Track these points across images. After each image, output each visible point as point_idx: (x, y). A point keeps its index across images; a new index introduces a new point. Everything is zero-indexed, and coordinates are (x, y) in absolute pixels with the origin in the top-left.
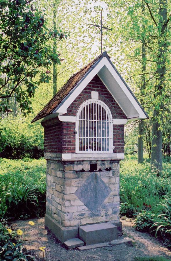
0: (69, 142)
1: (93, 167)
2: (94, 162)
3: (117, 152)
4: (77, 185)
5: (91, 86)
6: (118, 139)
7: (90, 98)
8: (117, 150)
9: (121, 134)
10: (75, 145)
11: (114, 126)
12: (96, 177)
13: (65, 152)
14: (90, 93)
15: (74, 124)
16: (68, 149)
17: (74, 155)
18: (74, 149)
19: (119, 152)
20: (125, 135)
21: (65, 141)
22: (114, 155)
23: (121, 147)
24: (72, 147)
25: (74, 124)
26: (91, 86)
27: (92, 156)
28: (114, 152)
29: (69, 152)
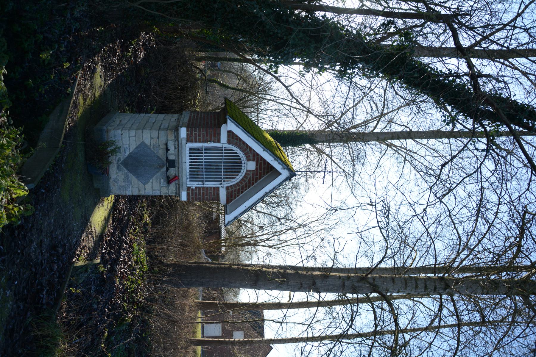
0: (199, 136)
1: (172, 164)
2: (177, 165)
6: (203, 193)
10: (196, 142)
11: (218, 188)
12: (161, 167)
13: (188, 131)
14: (254, 160)
15: (219, 142)
16: (192, 133)
17: (184, 142)
18: (192, 142)
21: (199, 131)
22: (185, 188)
25: (219, 142)
28: (189, 188)
29: (188, 135)
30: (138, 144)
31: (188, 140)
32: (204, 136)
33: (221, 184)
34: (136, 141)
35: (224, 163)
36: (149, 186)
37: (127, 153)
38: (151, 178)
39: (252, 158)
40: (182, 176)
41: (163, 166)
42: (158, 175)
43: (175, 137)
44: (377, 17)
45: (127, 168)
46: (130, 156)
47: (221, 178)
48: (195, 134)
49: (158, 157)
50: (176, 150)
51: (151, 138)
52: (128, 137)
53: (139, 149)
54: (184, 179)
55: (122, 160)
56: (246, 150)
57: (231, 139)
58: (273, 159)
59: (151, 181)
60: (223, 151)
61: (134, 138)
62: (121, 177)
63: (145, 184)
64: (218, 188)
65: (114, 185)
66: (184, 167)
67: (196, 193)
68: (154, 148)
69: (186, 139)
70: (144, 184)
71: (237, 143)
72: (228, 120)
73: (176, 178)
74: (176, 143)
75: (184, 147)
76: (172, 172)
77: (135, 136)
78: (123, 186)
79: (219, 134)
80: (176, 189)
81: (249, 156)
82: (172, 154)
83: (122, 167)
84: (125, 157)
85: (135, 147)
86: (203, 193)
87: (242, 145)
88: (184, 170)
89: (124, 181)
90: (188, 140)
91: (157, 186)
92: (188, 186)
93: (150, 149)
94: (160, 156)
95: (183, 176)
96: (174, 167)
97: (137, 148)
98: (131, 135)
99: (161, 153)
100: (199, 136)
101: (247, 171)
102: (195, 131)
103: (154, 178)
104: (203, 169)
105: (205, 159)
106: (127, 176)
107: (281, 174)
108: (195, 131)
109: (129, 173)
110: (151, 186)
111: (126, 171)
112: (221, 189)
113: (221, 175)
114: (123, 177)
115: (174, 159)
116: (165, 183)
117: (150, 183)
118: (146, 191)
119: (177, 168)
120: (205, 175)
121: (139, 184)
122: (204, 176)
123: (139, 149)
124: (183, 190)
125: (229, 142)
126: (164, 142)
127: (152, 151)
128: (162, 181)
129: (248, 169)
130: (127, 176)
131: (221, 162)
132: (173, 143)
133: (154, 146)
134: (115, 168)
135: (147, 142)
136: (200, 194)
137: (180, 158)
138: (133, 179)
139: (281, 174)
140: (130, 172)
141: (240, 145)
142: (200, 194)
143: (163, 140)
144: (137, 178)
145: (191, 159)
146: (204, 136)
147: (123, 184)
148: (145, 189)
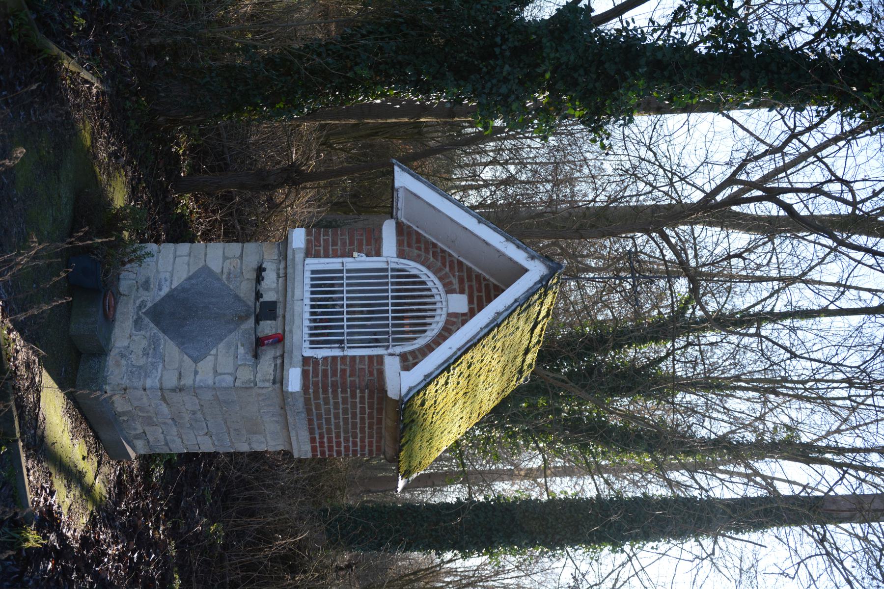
0: (334, 243)
1: (268, 311)
2: (280, 311)
3: (306, 368)
4: (225, 271)
5: (333, 379)
6: (343, 371)
7: (449, 291)
8: (311, 368)
9: (357, 381)
10: (327, 256)
11: (380, 358)
12: (242, 319)
13: (308, 234)
14: (462, 292)
15: (378, 253)
16: (317, 239)
17: (300, 256)
18: (317, 256)
19: (305, 374)
20: (499, 399)
21: (335, 234)
22: (297, 359)
23: (367, 245)
24: (321, 248)
25: (378, 253)
26: (333, 379)
27: (296, 298)
28: (306, 360)
29: (308, 242)
30: (193, 269)
31: (308, 254)
32: (344, 244)
33: (387, 347)
34: (188, 264)
35: (393, 298)
36: (206, 366)
37: (165, 290)
38: (215, 345)
39: (456, 286)
40: (291, 331)
41: (247, 317)
42: (234, 337)
43: (280, 254)
44: (659, 116)
45: (157, 323)
46: (169, 296)
47: (387, 333)
48: (326, 241)
49: (237, 298)
50: (281, 280)
51: (225, 258)
52: (171, 256)
53: (193, 282)
54: (296, 338)
55: (149, 305)
56: (440, 270)
57: (406, 248)
58: (504, 239)
59: (213, 352)
60: (390, 273)
61: (187, 258)
62: (140, 342)
63: (196, 361)
64: (380, 358)
65: (118, 365)
66: (297, 309)
67: (325, 372)
68: (228, 278)
69: (303, 251)
70: (196, 361)
71: (419, 256)
72: (396, 168)
73: (279, 339)
74: (282, 266)
75: (300, 267)
76: (268, 328)
77: (189, 255)
78: (140, 367)
79: (379, 240)
80: (275, 370)
81: (451, 283)
82: (270, 289)
83: (147, 320)
84: (158, 299)
85: (184, 276)
86: (343, 371)
87: (432, 259)
88: (296, 318)
89: (146, 354)
90: (308, 254)
91: (226, 364)
92: (305, 354)
93: (219, 279)
94: (242, 295)
95: (295, 329)
96: (274, 318)
97: (190, 278)
98: (178, 253)
99: (245, 290)
100: (334, 243)
101: (449, 315)
102: (326, 234)
103: (221, 346)
104: (342, 306)
105: (348, 292)
106: (154, 342)
107: (527, 270)
108: (326, 234)
109: (161, 335)
110: (211, 364)
111: (155, 330)
112: (388, 360)
113: (387, 326)
114: (144, 343)
115: (274, 299)
116: (249, 357)
117: (209, 358)
118: (198, 378)
119: (280, 319)
120: (349, 327)
121: (182, 361)
122: (346, 330)
123: (193, 282)
124: (292, 365)
125: (401, 254)
126: (255, 265)
127: (225, 284)
128: (241, 350)
129: (451, 311)
130: (154, 342)
131: (387, 298)
132: (274, 267)
133: (229, 274)
134: (129, 324)
135: (215, 265)
136: (334, 374)
137: (289, 290)
138: (170, 348)
139: (527, 270)
140: (164, 332)
141: (427, 259)
142: (334, 374)
143: (251, 261)
144: (180, 345)
145: (315, 321)
146: (344, 244)
147: (142, 362)
148: (196, 373)
